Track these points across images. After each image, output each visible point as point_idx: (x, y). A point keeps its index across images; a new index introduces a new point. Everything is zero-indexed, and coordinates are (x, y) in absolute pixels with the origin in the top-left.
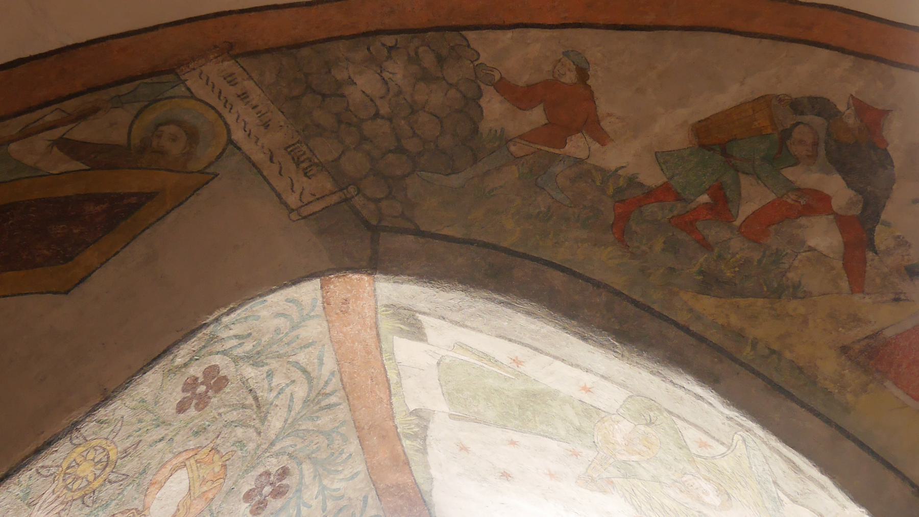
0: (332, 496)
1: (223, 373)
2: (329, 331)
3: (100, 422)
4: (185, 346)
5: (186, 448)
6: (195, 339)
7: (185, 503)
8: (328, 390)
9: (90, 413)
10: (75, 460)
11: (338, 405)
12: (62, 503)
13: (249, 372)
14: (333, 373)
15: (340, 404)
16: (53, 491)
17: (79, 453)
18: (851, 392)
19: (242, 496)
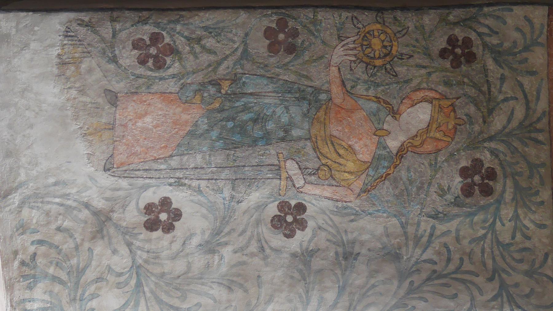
0: (521, 229)
1: (474, 49)
2: (548, 66)
3: (395, 18)
4: (458, 10)
5: (437, 89)
6: (464, 10)
7: (422, 134)
8: (539, 126)
9: (394, 9)
10: (373, 31)
11: (543, 144)
12: (355, 55)
13: (491, 64)
14: (544, 113)
15: (544, 144)
16: (355, 41)
17: (377, 28)
18: (28, 128)
19: (459, 168)
